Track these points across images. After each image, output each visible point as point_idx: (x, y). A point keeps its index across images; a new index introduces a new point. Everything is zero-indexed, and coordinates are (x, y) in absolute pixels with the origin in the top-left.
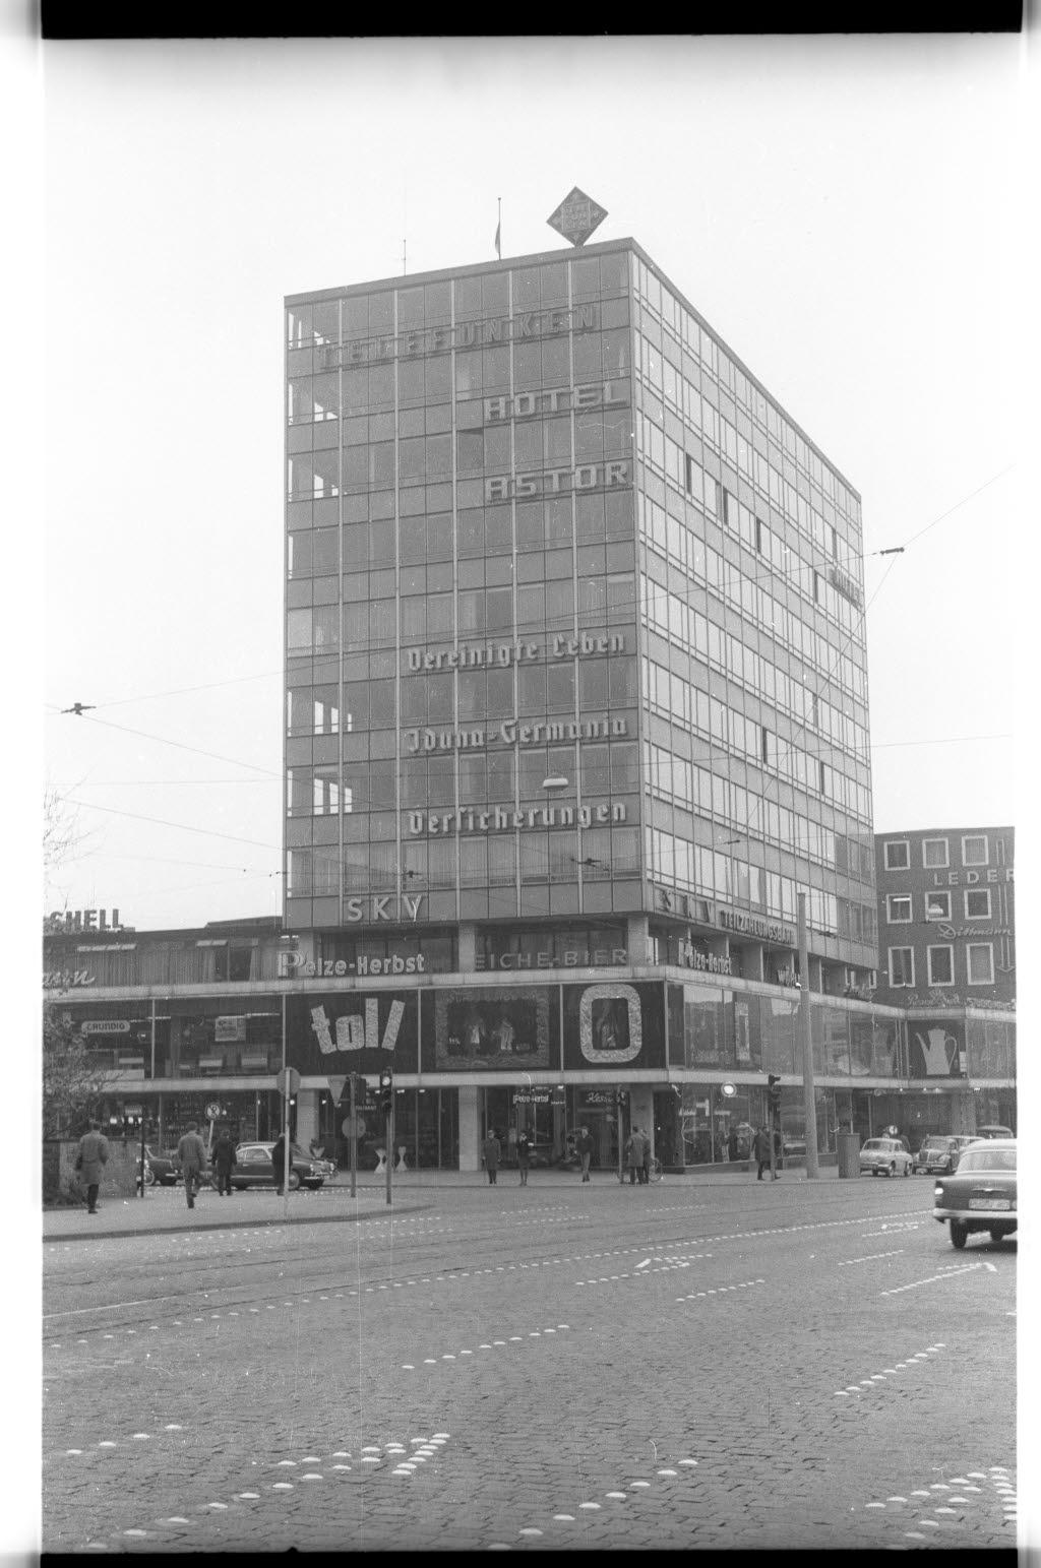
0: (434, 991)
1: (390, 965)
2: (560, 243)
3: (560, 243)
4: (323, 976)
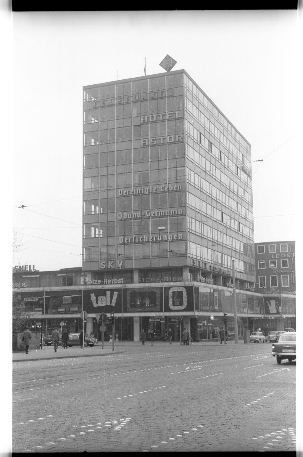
0: (126, 289)
1: (114, 281)
2: (163, 71)
3: (163, 71)
4: (94, 285)
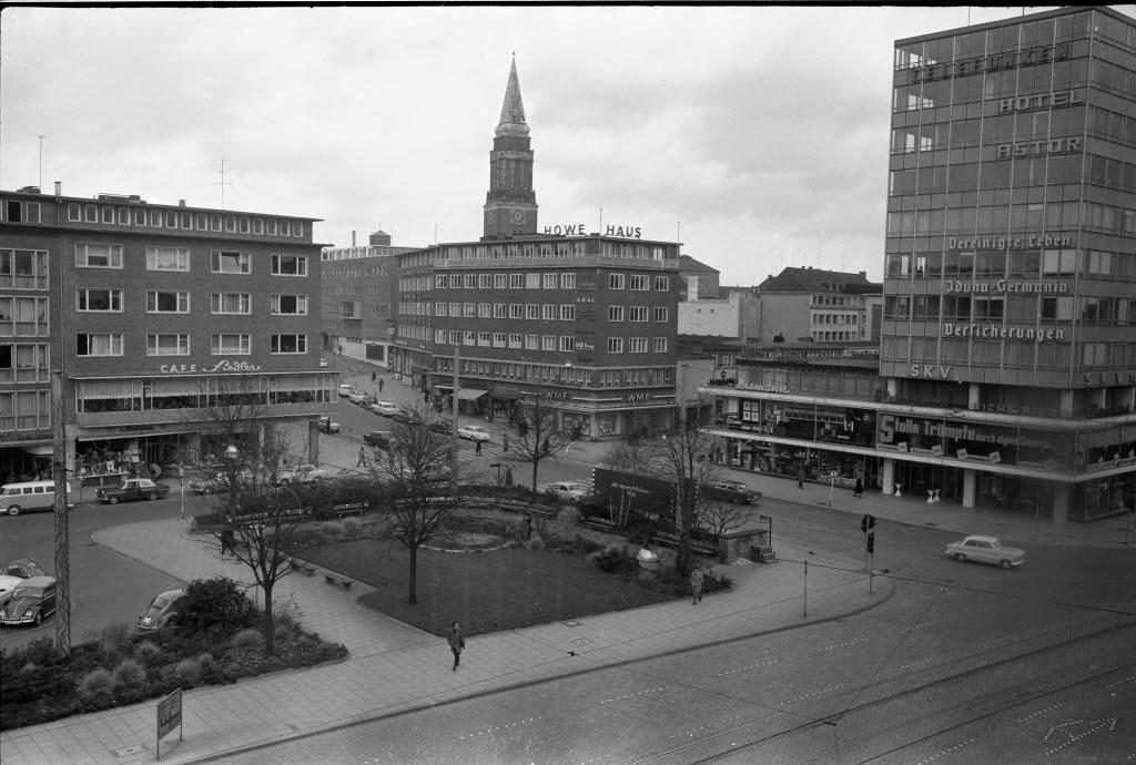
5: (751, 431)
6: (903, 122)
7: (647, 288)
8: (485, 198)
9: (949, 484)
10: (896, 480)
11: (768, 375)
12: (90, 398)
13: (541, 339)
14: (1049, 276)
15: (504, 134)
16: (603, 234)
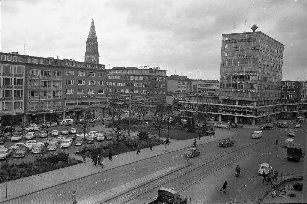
2: (252, 31)
3: (252, 31)
5: (191, 110)
6: (223, 50)
7: (161, 80)
8: (85, 54)
9: (232, 119)
10: (221, 119)
11: (193, 99)
12: (69, 102)
13: (138, 91)
14: (252, 80)
15: (90, 37)
16: (153, 68)
